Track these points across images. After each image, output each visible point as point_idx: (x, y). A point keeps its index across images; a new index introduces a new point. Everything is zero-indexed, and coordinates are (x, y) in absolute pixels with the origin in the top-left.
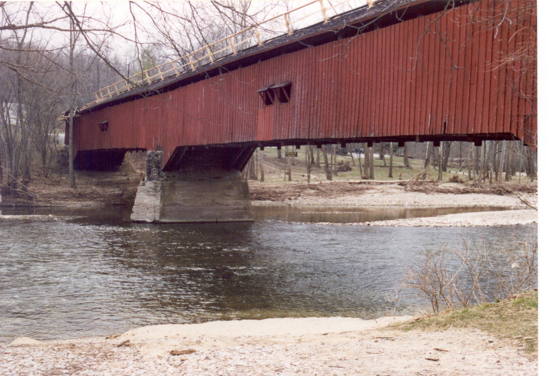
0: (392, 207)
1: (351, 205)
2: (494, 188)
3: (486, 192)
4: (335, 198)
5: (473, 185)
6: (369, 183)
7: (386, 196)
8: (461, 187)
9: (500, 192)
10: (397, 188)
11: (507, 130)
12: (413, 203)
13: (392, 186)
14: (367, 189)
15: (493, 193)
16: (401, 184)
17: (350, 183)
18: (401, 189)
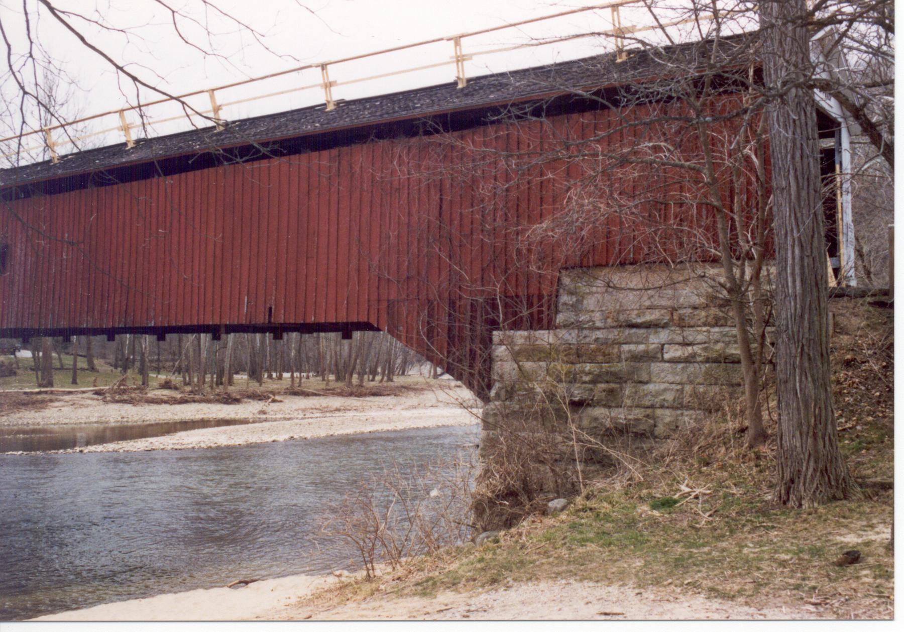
0: (91, 425)
1: (34, 424)
2: (218, 395)
3: (208, 401)
4: (7, 415)
5: (191, 392)
6: (52, 393)
7: (80, 410)
8: (178, 395)
9: (229, 400)
10: (92, 399)
11: (363, 319)
12: (119, 419)
13: (84, 395)
14: (51, 401)
15: (219, 401)
16: (97, 393)
17: (26, 393)
18: (98, 400)
